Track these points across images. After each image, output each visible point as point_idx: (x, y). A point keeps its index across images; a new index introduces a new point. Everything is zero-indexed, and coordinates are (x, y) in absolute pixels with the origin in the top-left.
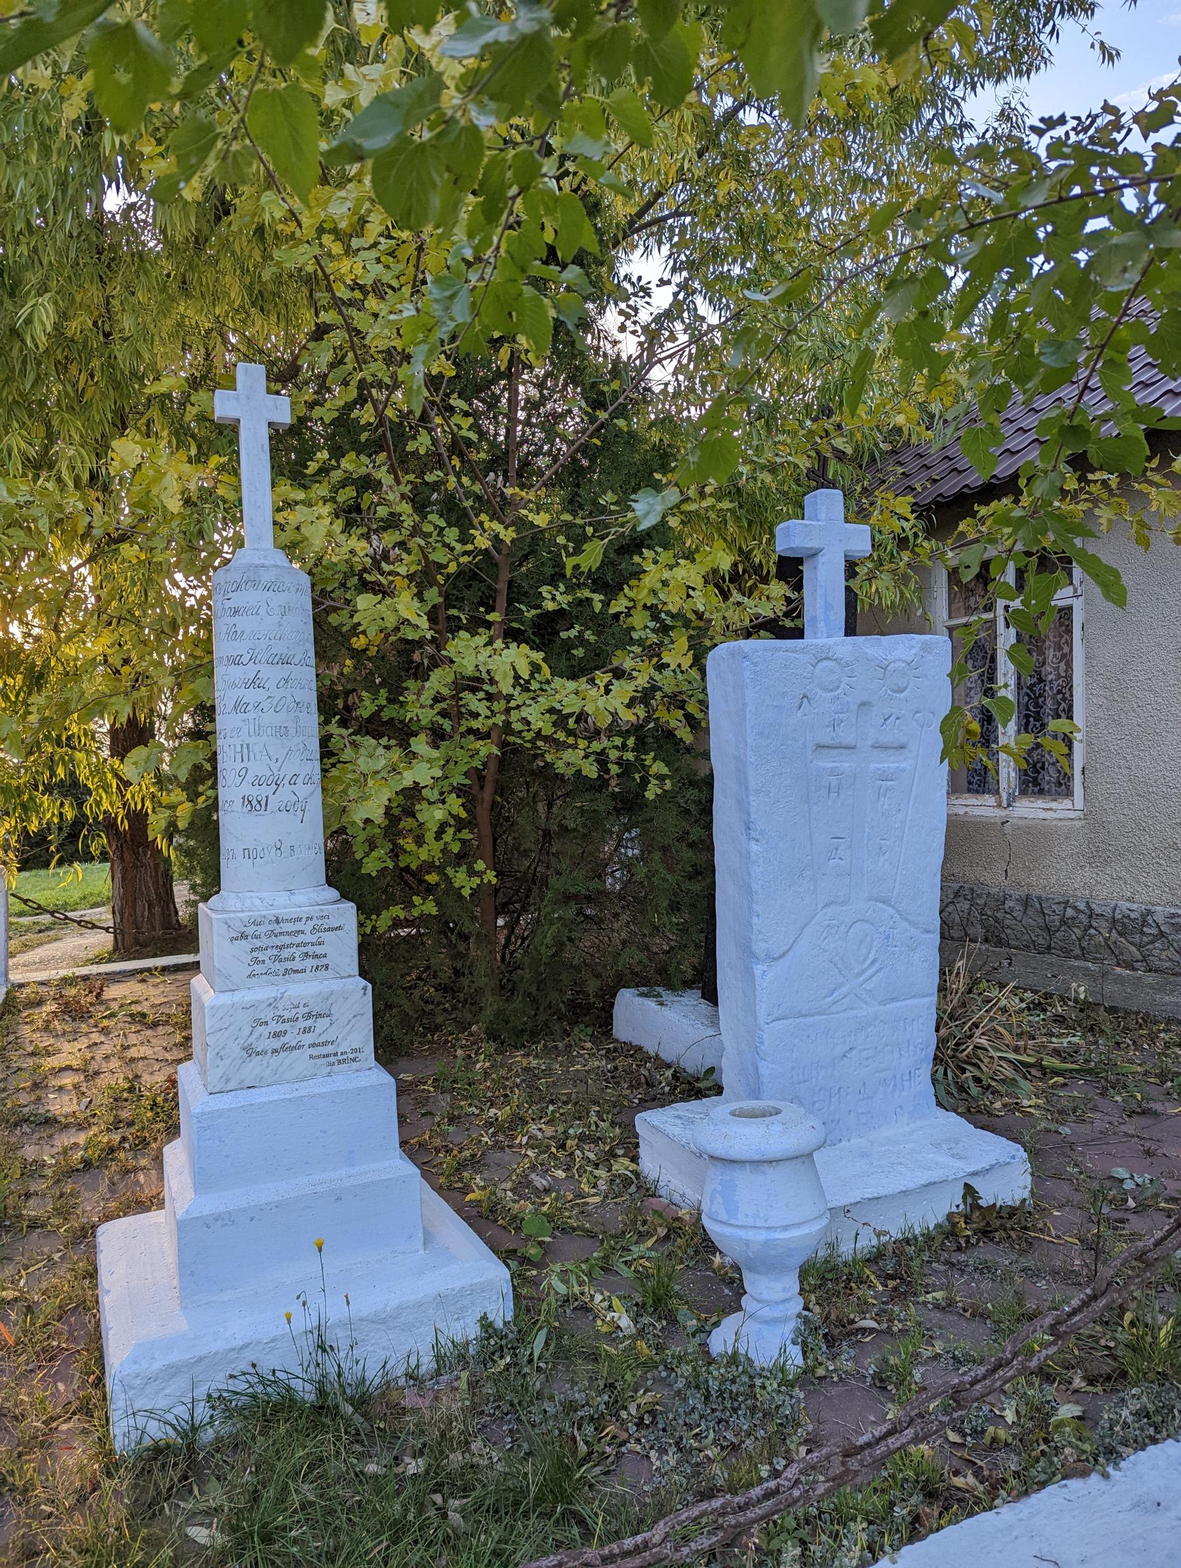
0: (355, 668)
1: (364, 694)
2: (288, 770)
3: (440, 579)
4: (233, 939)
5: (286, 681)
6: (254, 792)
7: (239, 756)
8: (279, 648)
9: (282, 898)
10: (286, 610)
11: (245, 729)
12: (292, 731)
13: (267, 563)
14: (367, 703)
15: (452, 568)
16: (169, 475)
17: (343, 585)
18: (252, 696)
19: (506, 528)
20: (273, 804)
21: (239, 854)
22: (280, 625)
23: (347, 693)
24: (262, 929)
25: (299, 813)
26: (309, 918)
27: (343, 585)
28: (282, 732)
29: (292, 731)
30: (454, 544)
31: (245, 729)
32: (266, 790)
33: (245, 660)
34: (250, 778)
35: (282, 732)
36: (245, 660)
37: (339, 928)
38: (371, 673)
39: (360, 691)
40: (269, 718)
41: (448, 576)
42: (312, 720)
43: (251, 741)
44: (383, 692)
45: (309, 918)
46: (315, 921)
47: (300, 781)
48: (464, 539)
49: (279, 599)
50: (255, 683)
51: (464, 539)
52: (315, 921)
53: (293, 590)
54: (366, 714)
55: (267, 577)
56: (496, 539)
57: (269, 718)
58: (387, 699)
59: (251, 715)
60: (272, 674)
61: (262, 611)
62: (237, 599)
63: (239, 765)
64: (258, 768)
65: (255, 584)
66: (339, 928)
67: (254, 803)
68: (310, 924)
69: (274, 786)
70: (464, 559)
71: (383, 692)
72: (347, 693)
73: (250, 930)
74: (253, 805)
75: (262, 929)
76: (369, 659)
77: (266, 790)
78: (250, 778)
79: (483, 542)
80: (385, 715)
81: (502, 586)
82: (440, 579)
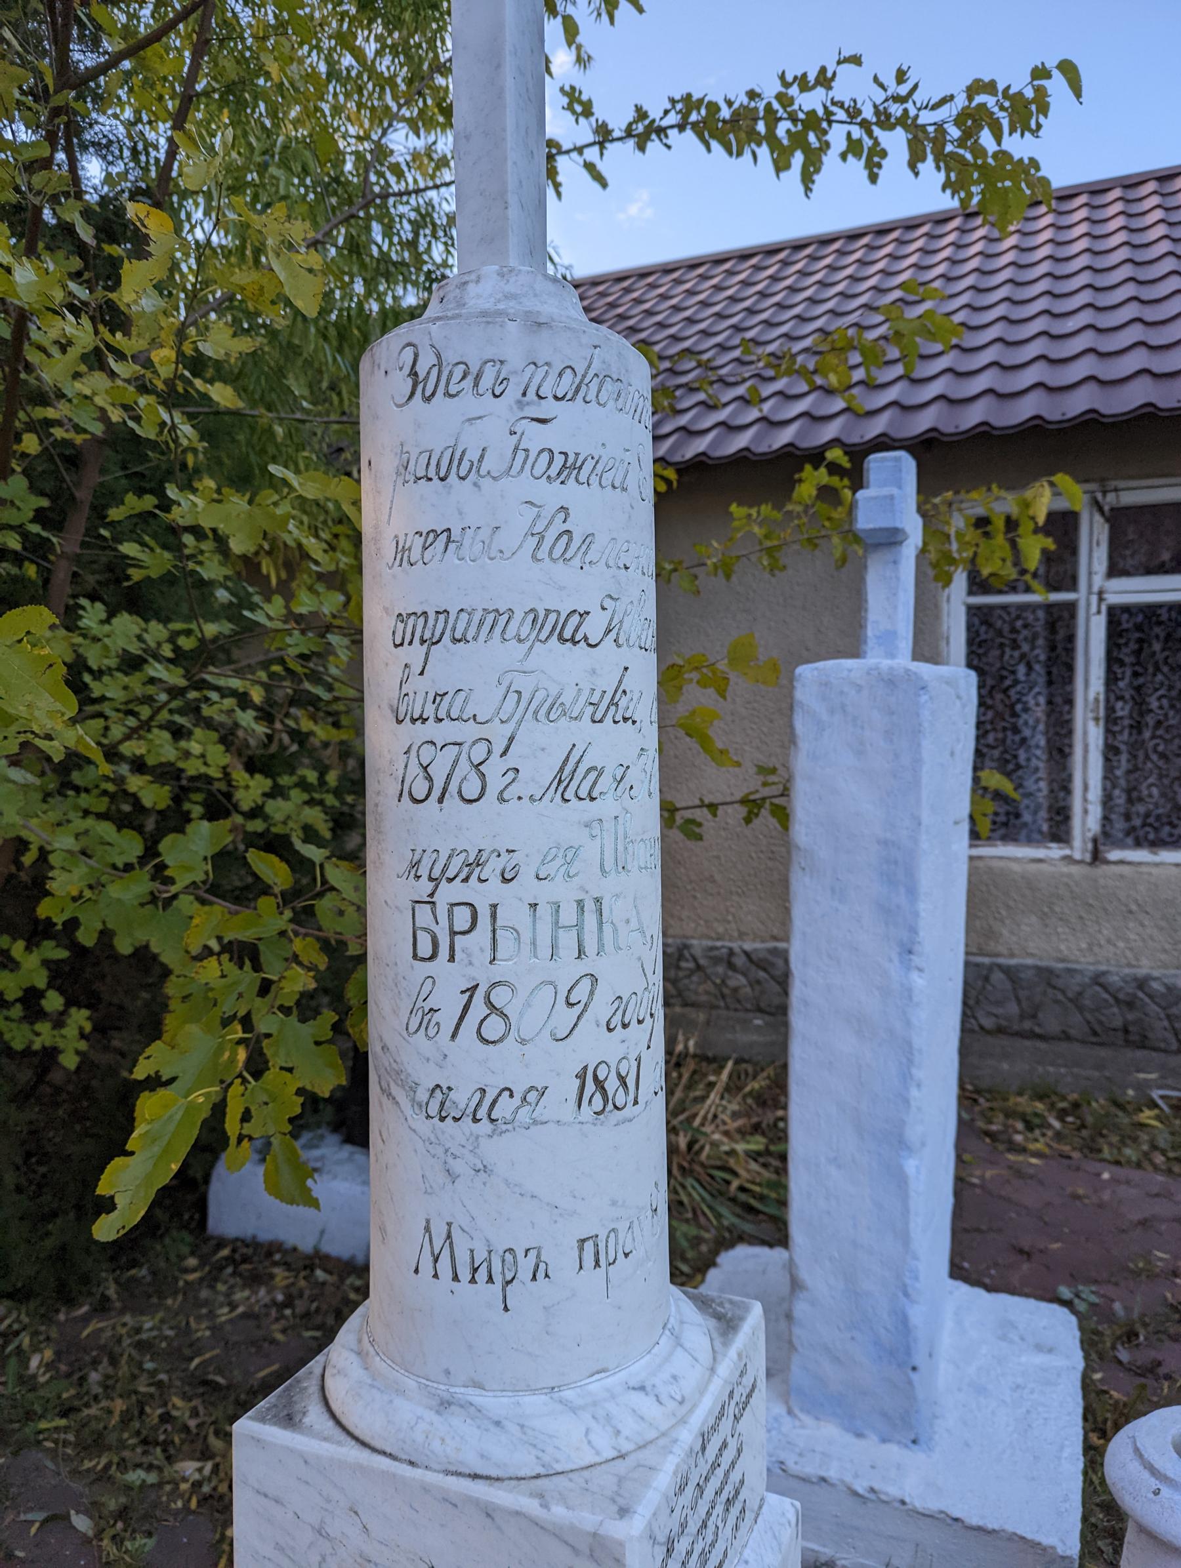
11: (591, 851)
36: (594, 627)
43: (606, 887)
67: (612, 1085)
78: (601, 1009)
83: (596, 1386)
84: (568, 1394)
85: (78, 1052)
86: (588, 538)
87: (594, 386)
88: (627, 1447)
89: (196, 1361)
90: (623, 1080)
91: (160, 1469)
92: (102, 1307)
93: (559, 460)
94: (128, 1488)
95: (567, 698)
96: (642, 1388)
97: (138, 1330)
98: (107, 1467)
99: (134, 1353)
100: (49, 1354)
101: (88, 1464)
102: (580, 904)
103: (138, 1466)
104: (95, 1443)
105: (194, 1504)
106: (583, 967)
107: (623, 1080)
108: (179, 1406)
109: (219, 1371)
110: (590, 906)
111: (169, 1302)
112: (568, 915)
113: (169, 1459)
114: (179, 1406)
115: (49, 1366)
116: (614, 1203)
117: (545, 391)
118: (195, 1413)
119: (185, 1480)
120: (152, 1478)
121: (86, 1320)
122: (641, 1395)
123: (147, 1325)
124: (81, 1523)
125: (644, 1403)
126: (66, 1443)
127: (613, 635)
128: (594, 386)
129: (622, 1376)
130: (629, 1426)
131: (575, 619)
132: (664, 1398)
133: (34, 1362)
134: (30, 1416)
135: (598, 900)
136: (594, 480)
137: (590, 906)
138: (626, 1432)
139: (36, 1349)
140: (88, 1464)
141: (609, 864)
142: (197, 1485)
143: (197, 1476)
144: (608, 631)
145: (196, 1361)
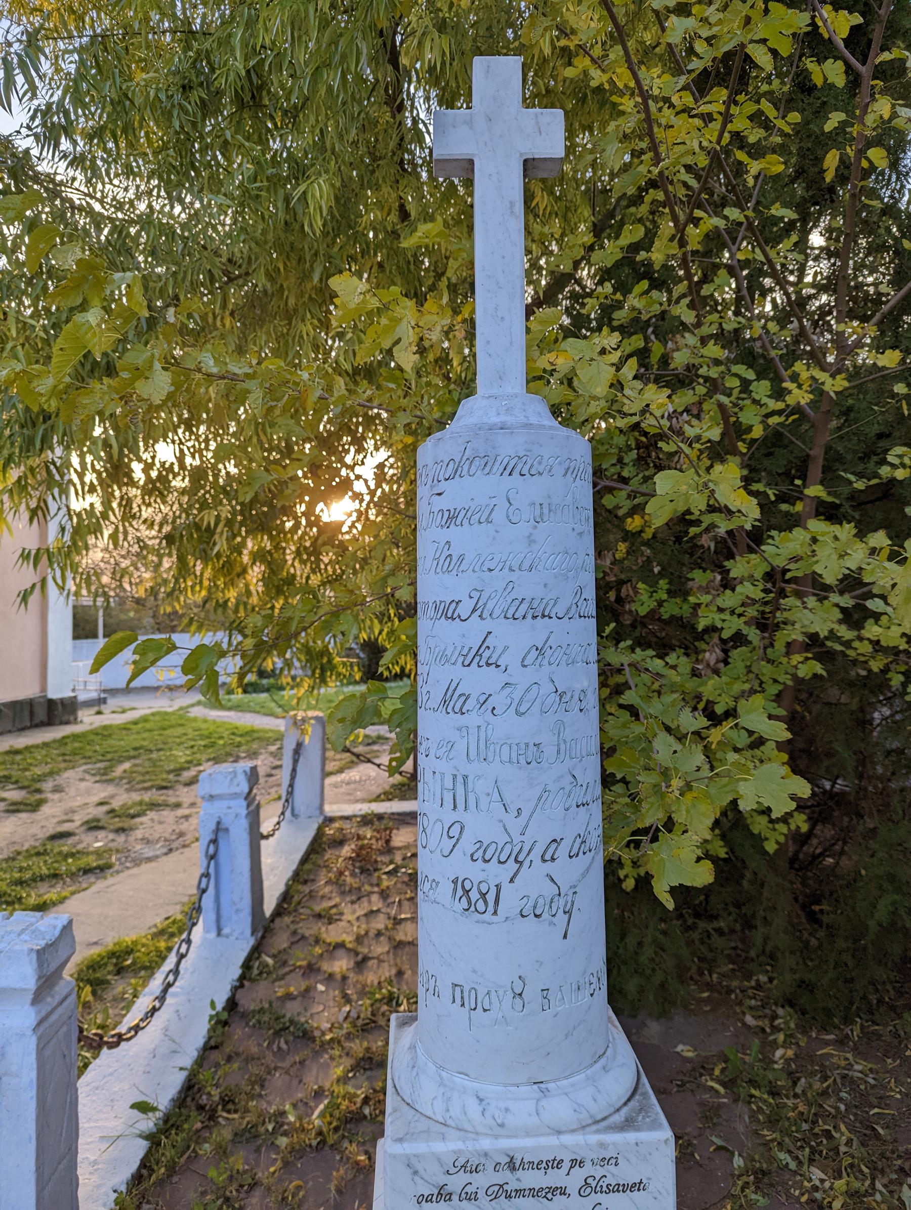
0: (628, 553)
1: (640, 585)
2: (540, 833)
3: (742, 447)
4: (422, 1199)
5: (540, 651)
6: (474, 872)
7: (448, 798)
8: (529, 587)
9: (521, 1107)
10: (543, 512)
11: (461, 746)
12: (550, 751)
13: (510, 420)
14: (644, 597)
15: (758, 432)
16: (404, 324)
17: (620, 461)
18: (476, 681)
19: (833, 376)
20: (510, 901)
21: (446, 992)
22: (531, 540)
23: (621, 583)
24: (481, 1181)
25: (561, 918)
26: (577, 1163)
27: (620, 461)
28: (530, 755)
29: (550, 751)
30: (765, 400)
31: (461, 746)
32: (497, 873)
33: (464, 610)
34: (467, 844)
35: (530, 755)
36: (464, 610)
37: (638, 1186)
38: (649, 561)
39: (648, 596)
40: (506, 727)
41: (754, 441)
42: (582, 633)
43: (472, 769)
44: (663, 584)
45: (577, 1163)
46: (588, 1170)
47: (562, 851)
48: (779, 393)
49: (530, 491)
50: (480, 656)
51: (779, 393)
52: (588, 1170)
53: (559, 470)
54: (643, 611)
55: (508, 447)
56: (817, 390)
57: (506, 727)
58: (669, 592)
59: (473, 719)
60: (513, 639)
61: (499, 516)
62: (456, 495)
63: (449, 816)
64: (483, 826)
65: (487, 462)
66: (638, 1186)
67: (474, 895)
68: (579, 1175)
69: (512, 866)
70: (774, 420)
71: (663, 584)
72: (621, 583)
73: (456, 1183)
74: (476, 900)
75: (481, 1181)
76: (647, 543)
77: (497, 873)
78: (467, 844)
79: (800, 396)
80: (666, 612)
81: (817, 452)
82: (742, 447)
83: (459, 1080)
84: (444, 1074)
85: (777, 843)
86: (461, 558)
87: (466, 467)
88: (450, 1122)
89: (876, 1110)
90: (483, 896)
91: (800, 1163)
92: (841, 1042)
93: (446, 514)
94: (772, 1159)
95: (448, 652)
96: (481, 1100)
97: (850, 1067)
98: (773, 1140)
99: (839, 1080)
100: (790, 1053)
101: (765, 1132)
102: (455, 776)
103: (789, 1152)
104: (773, 1122)
105: (804, 1199)
106: (455, 816)
107: (483, 896)
108: (843, 1135)
109: (886, 1127)
110: (460, 779)
111: (889, 1061)
112: (449, 784)
113: (811, 1161)
114: (843, 1135)
115: (788, 1061)
116: (474, 971)
117: (441, 478)
118: (849, 1143)
119: (810, 1180)
120: (793, 1165)
121: (827, 1043)
122: (477, 1102)
123: (857, 1067)
124: (738, 1162)
125: (474, 1108)
126: (763, 1113)
127: (478, 613)
128: (466, 467)
129: (476, 1085)
130: (456, 1111)
131: (453, 605)
132: (487, 1114)
133: (779, 1053)
134: (752, 1083)
135: (465, 778)
136: (465, 522)
137: (460, 779)
138: (452, 1113)
139: (785, 1045)
140: (765, 1132)
141: (473, 755)
142: (816, 1189)
143: (818, 1183)
144: (474, 610)
145: (876, 1110)
